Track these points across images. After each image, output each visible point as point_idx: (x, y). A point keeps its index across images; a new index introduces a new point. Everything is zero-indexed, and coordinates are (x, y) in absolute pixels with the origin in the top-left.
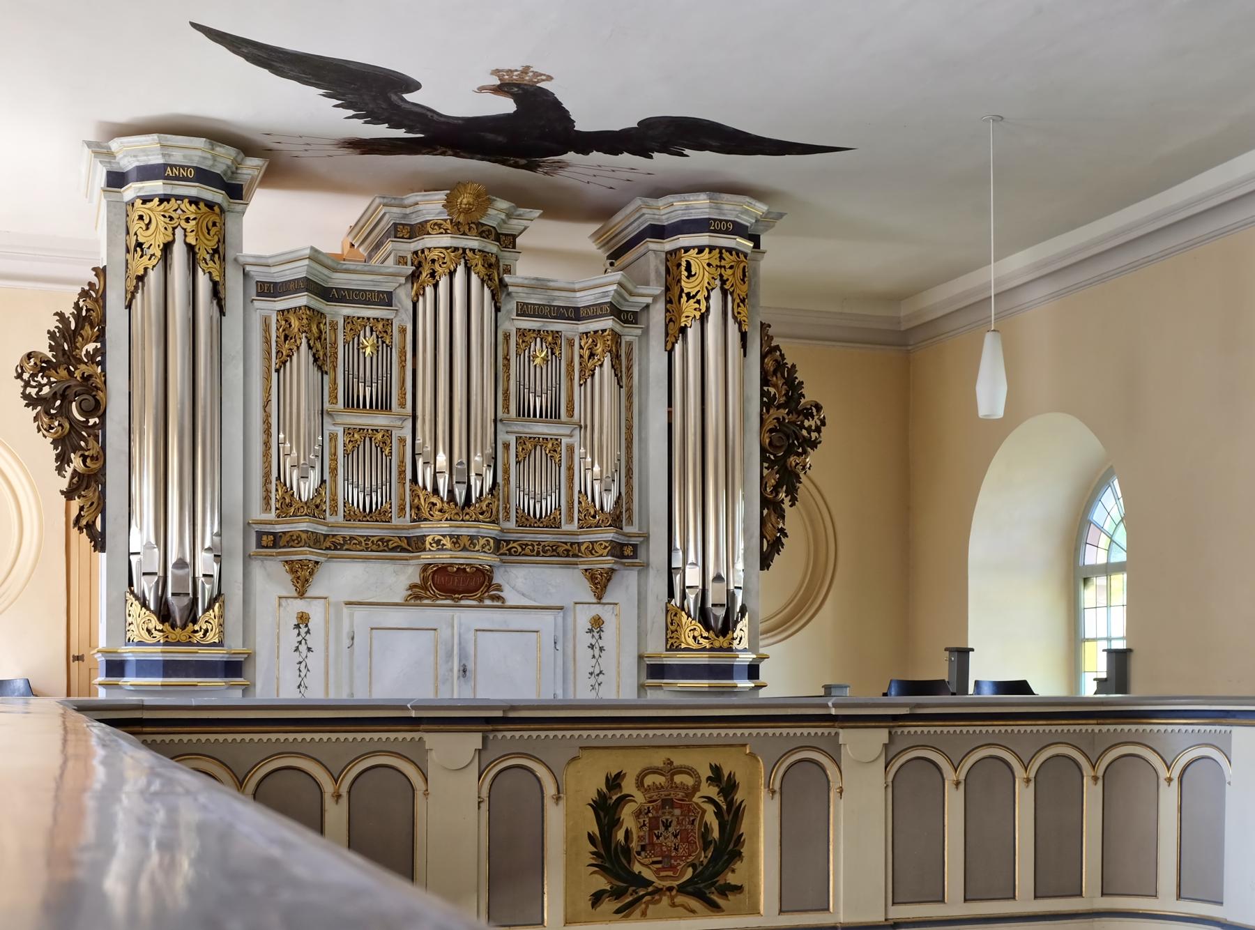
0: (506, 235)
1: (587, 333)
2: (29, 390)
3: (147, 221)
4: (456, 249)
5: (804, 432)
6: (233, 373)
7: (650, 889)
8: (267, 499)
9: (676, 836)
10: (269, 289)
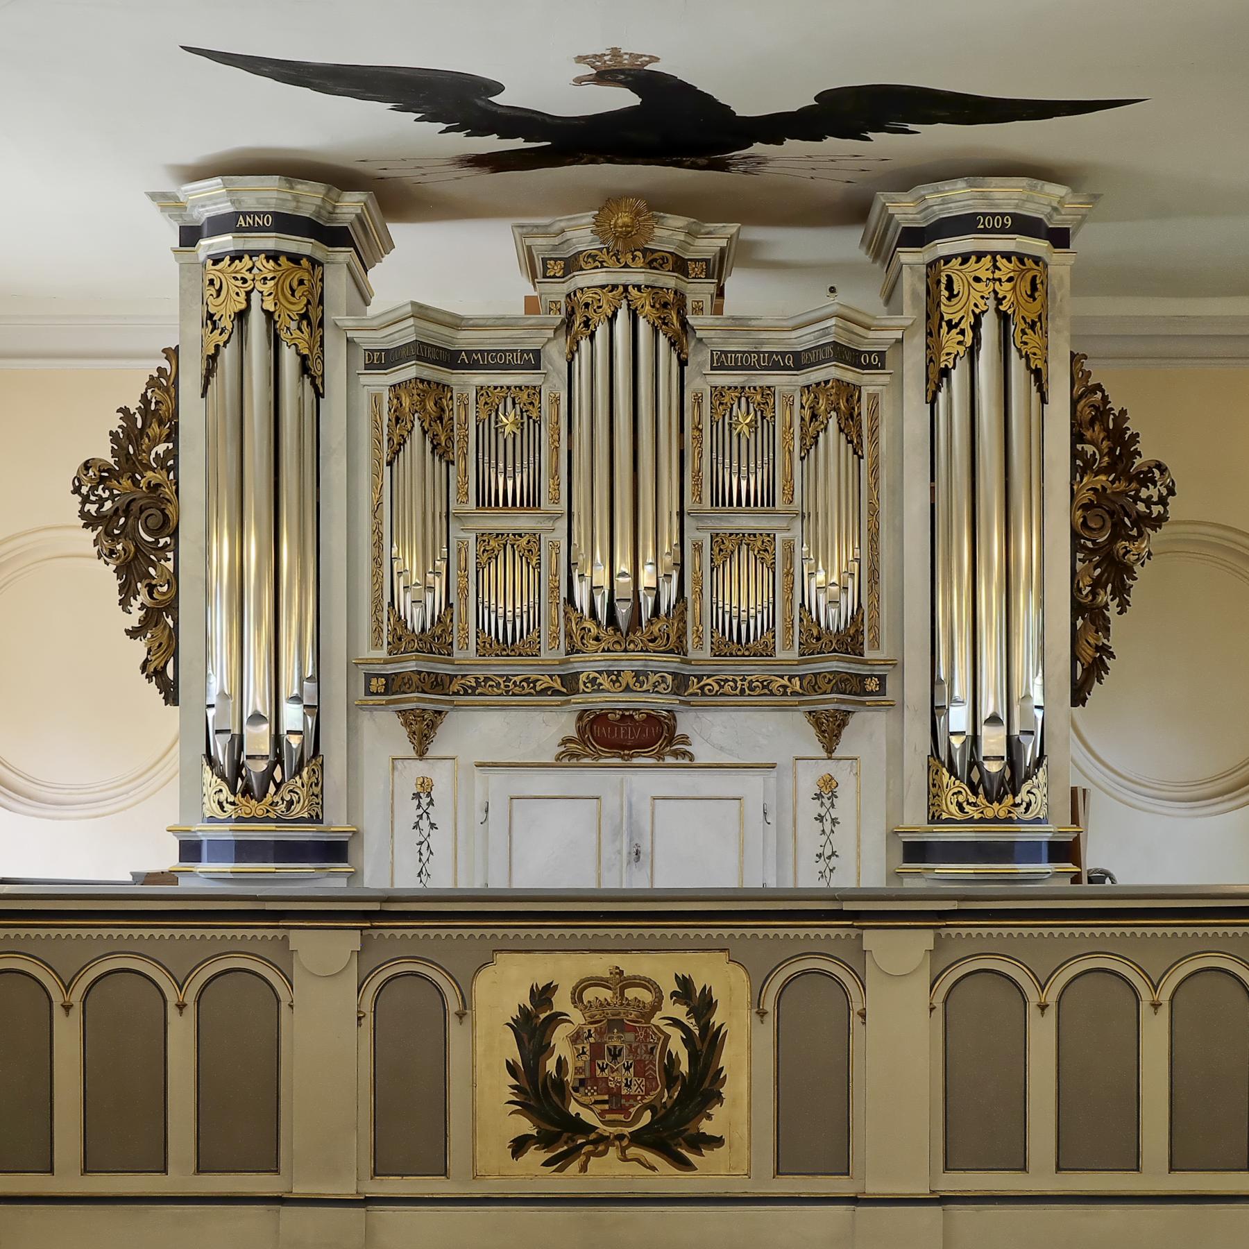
1: (808, 387)
2: (88, 507)
3: (217, 287)
4: (615, 287)
5: (1141, 507)
6: (335, 470)
7: (593, 1136)
8: (378, 631)
9: (628, 1069)
10: (380, 358)
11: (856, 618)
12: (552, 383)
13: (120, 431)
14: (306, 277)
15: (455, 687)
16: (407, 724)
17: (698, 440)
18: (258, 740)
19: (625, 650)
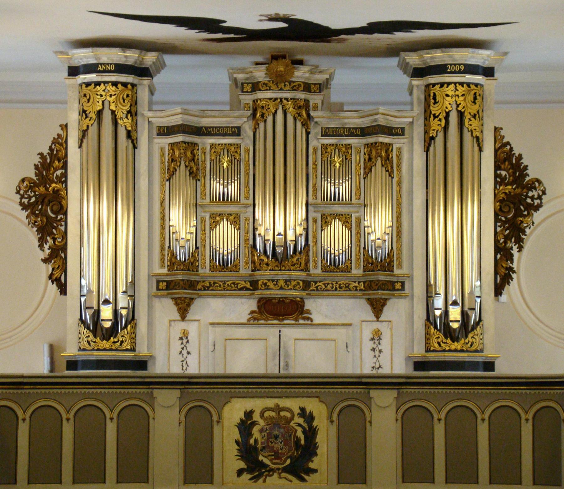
0: (315, 84)
1: (367, 145)
2: (23, 200)
3: (88, 97)
4: (276, 99)
5: (529, 200)
6: (143, 183)
7: (268, 469)
8: (162, 260)
9: (281, 443)
10: (164, 131)
11: (390, 255)
12: (246, 142)
13: (39, 164)
14: (130, 93)
15: (199, 287)
16: (177, 304)
17: (315, 169)
18: (107, 313)
19: (280, 270)
